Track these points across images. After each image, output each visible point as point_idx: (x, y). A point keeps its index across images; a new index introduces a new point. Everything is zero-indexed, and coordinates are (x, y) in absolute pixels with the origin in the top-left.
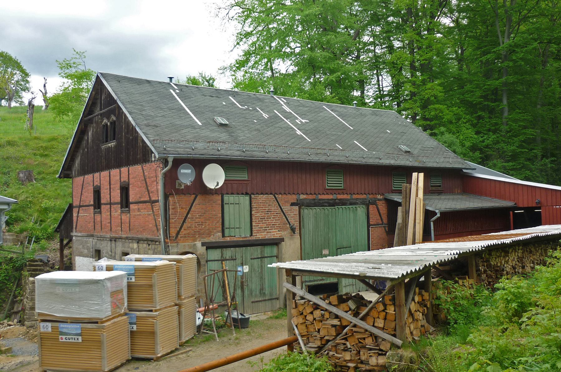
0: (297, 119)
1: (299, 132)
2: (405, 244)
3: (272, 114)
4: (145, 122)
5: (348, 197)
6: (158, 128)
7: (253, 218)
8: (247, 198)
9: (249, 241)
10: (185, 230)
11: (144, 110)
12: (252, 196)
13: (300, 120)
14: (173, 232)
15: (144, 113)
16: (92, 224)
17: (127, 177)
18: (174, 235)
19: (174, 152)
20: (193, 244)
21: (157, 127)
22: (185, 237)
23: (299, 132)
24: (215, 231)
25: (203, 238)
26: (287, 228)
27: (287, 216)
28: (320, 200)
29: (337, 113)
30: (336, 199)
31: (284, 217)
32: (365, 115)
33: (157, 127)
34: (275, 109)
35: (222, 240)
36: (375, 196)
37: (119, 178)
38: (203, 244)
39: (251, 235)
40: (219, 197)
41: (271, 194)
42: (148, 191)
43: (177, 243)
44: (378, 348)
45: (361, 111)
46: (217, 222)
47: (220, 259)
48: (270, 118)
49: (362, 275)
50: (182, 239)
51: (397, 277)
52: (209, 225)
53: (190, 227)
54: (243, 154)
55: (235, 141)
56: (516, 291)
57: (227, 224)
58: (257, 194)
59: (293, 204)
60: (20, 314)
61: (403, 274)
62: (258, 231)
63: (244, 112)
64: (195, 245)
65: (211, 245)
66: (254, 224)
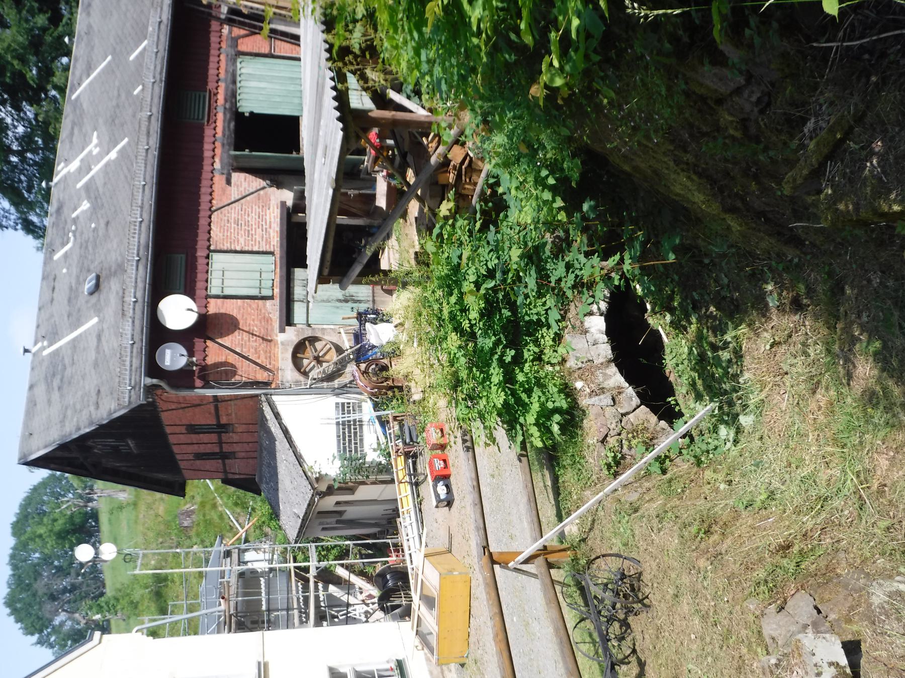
0: (91, 152)
1: (113, 155)
3: (83, 194)
4: (92, 408)
5: (222, 85)
6: (102, 390)
7: (246, 249)
8: (215, 257)
9: (281, 258)
10: (259, 358)
11: (74, 405)
12: (212, 248)
13: (93, 147)
14: (262, 376)
15: (78, 407)
16: (250, 461)
18: (266, 374)
19: (138, 374)
20: (280, 345)
21: (99, 391)
22: (270, 357)
23: (113, 155)
24: (263, 311)
25: (272, 330)
26: (266, 194)
27: (247, 193)
28: (224, 135)
29: (84, 77)
30: (225, 108)
31: (248, 198)
32: (90, 26)
33: (99, 391)
34: (75, 187)
35: (277, 301)
36: (224, 38)
37: (181, 436)
38: (282, 330)
39: (272, 253)
40: (212, 302)
41: (210, 217)
42: (199, 405)
43: (278, 369)
45: (83, 33)
46: (250, 306)
47: (305, 305)
48: (89, 198)
49: (334, 186)
50: (273, 362)
51: (341, 133)
52: (253, 320)
53: (256, 350)
54: (143, 261)
55: (121, 269)
58: (209, 240)
59: (229, 182)
61: (336, 108)
62: (268, 242)
63: (79, 240)
64: (282, 343)
65: (284, 319)
66: (256, 249)
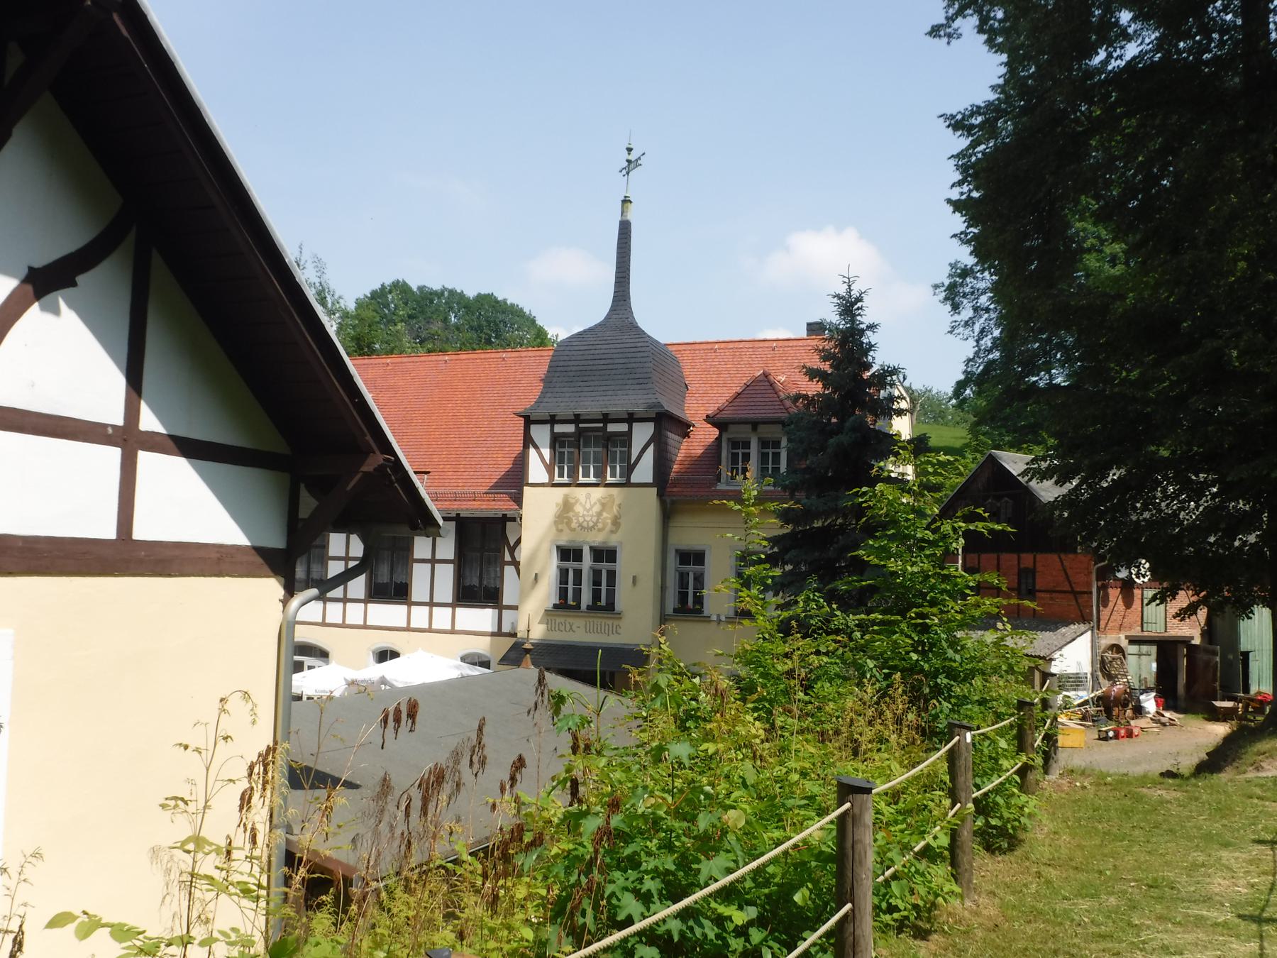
2: (749, 453)
14: (1102, 623)
17: (981, 561)
35: (1140, 634)
38: (1127, 637)
39: (1166, 631)
44: (581, 425)
56: (945, 644)
57: (1145, 620)
60: (1116, 656)
